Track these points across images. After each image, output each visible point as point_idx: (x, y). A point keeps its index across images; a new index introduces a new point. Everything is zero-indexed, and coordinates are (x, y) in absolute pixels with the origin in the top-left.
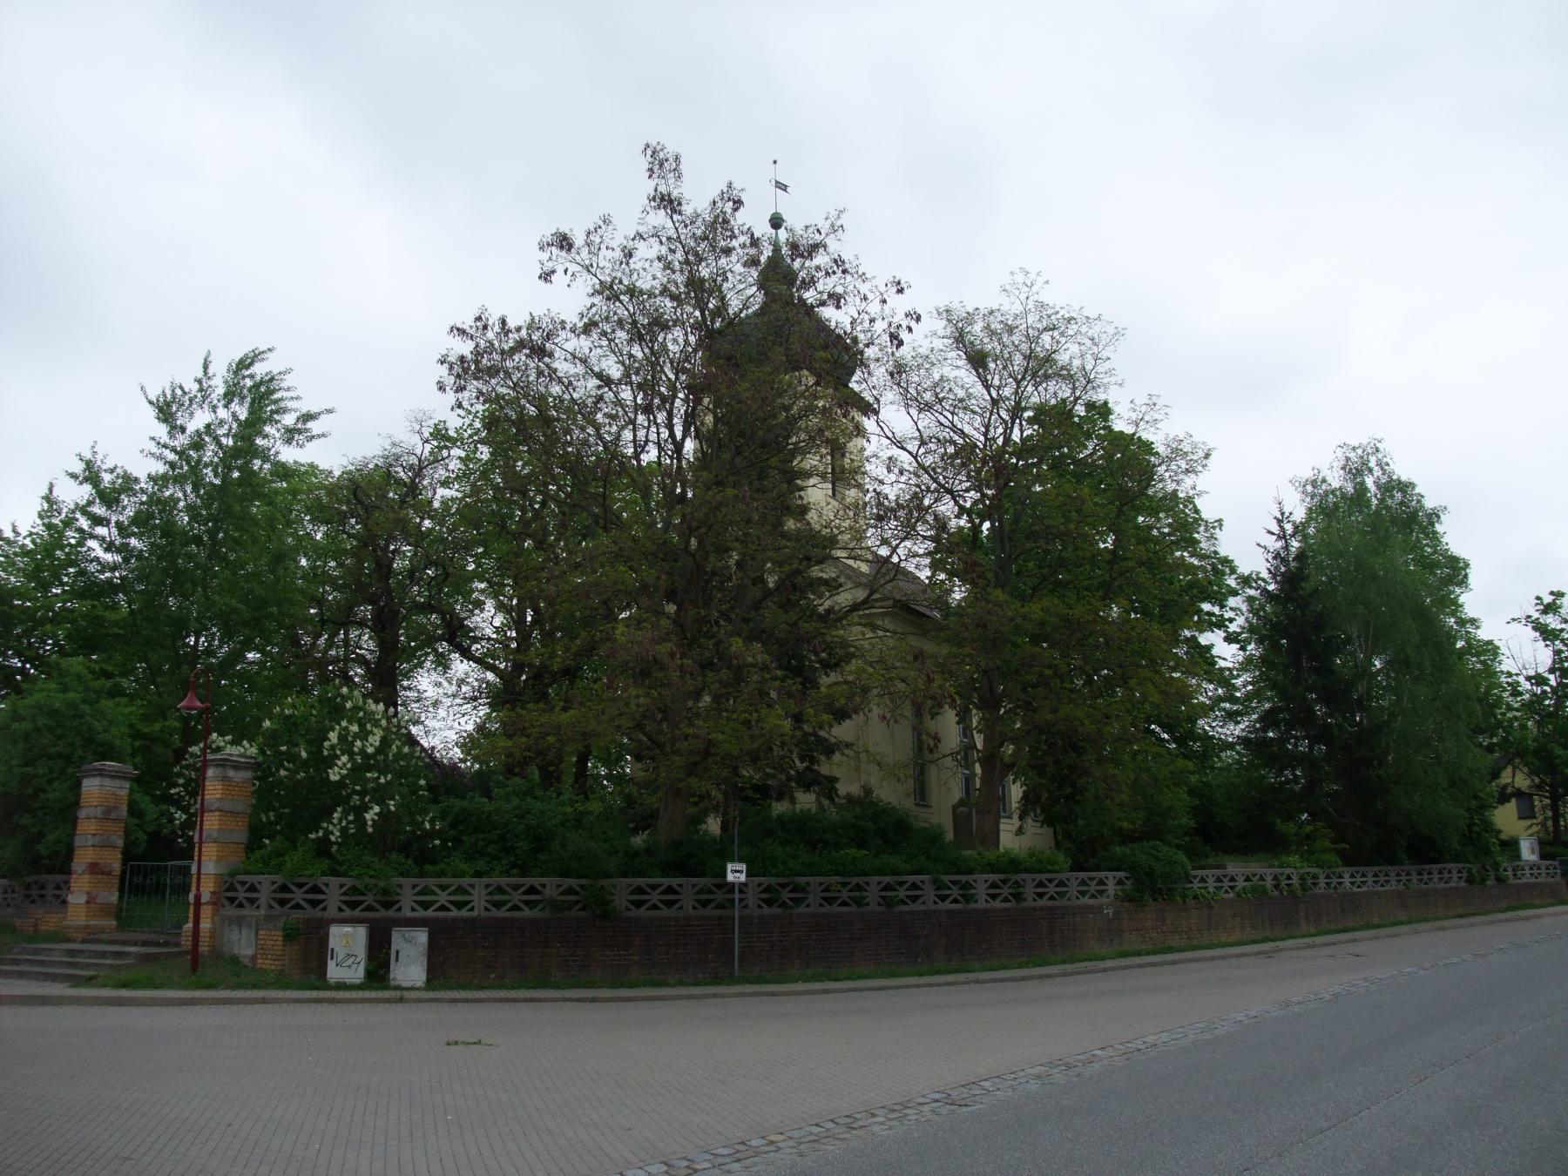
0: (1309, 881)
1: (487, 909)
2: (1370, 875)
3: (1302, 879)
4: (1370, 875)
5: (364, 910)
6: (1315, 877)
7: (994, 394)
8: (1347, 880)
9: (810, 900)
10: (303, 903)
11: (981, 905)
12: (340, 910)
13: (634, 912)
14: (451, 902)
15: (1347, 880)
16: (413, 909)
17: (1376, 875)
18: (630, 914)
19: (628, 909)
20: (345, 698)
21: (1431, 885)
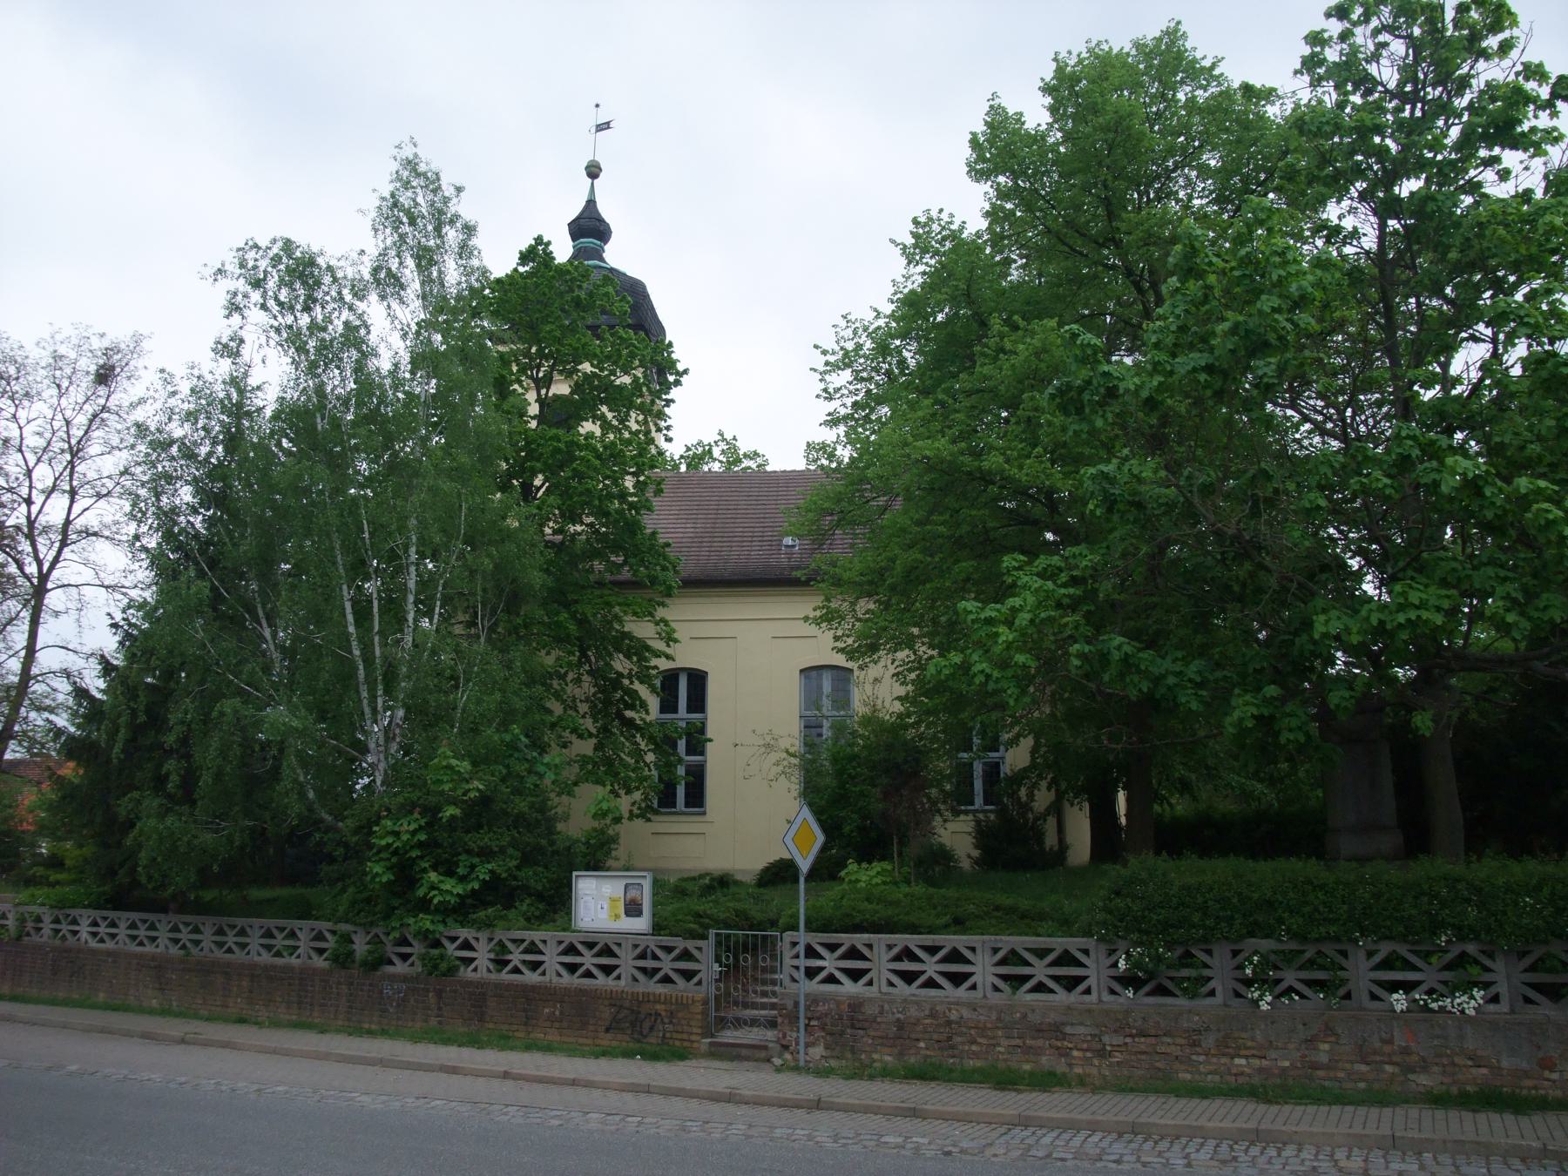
0: (30, 925)
1: (489, 971)
2: (123, 925)
3: (22, 920)
4: (123, 925)
5: (824, 981)
6: (39, 919)
7: (1121, 506)
8: (84, 930)
9: (886, 956)
10: (838, 974)
11: (482, 974)
12: (870, 946)
13: (1073, 944)
14: (1056, 978)
15: (84, 930)
16: (700, 949)
17: (133, 926)
18: (1081, 942)
19: (1086, 952)
20: (1387, 417)
21: (239, 956)
